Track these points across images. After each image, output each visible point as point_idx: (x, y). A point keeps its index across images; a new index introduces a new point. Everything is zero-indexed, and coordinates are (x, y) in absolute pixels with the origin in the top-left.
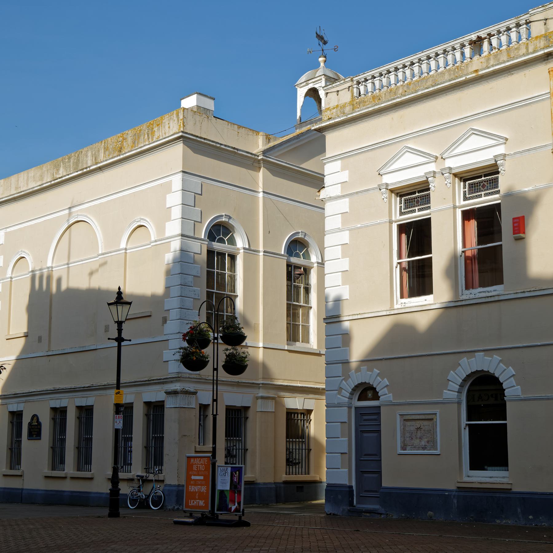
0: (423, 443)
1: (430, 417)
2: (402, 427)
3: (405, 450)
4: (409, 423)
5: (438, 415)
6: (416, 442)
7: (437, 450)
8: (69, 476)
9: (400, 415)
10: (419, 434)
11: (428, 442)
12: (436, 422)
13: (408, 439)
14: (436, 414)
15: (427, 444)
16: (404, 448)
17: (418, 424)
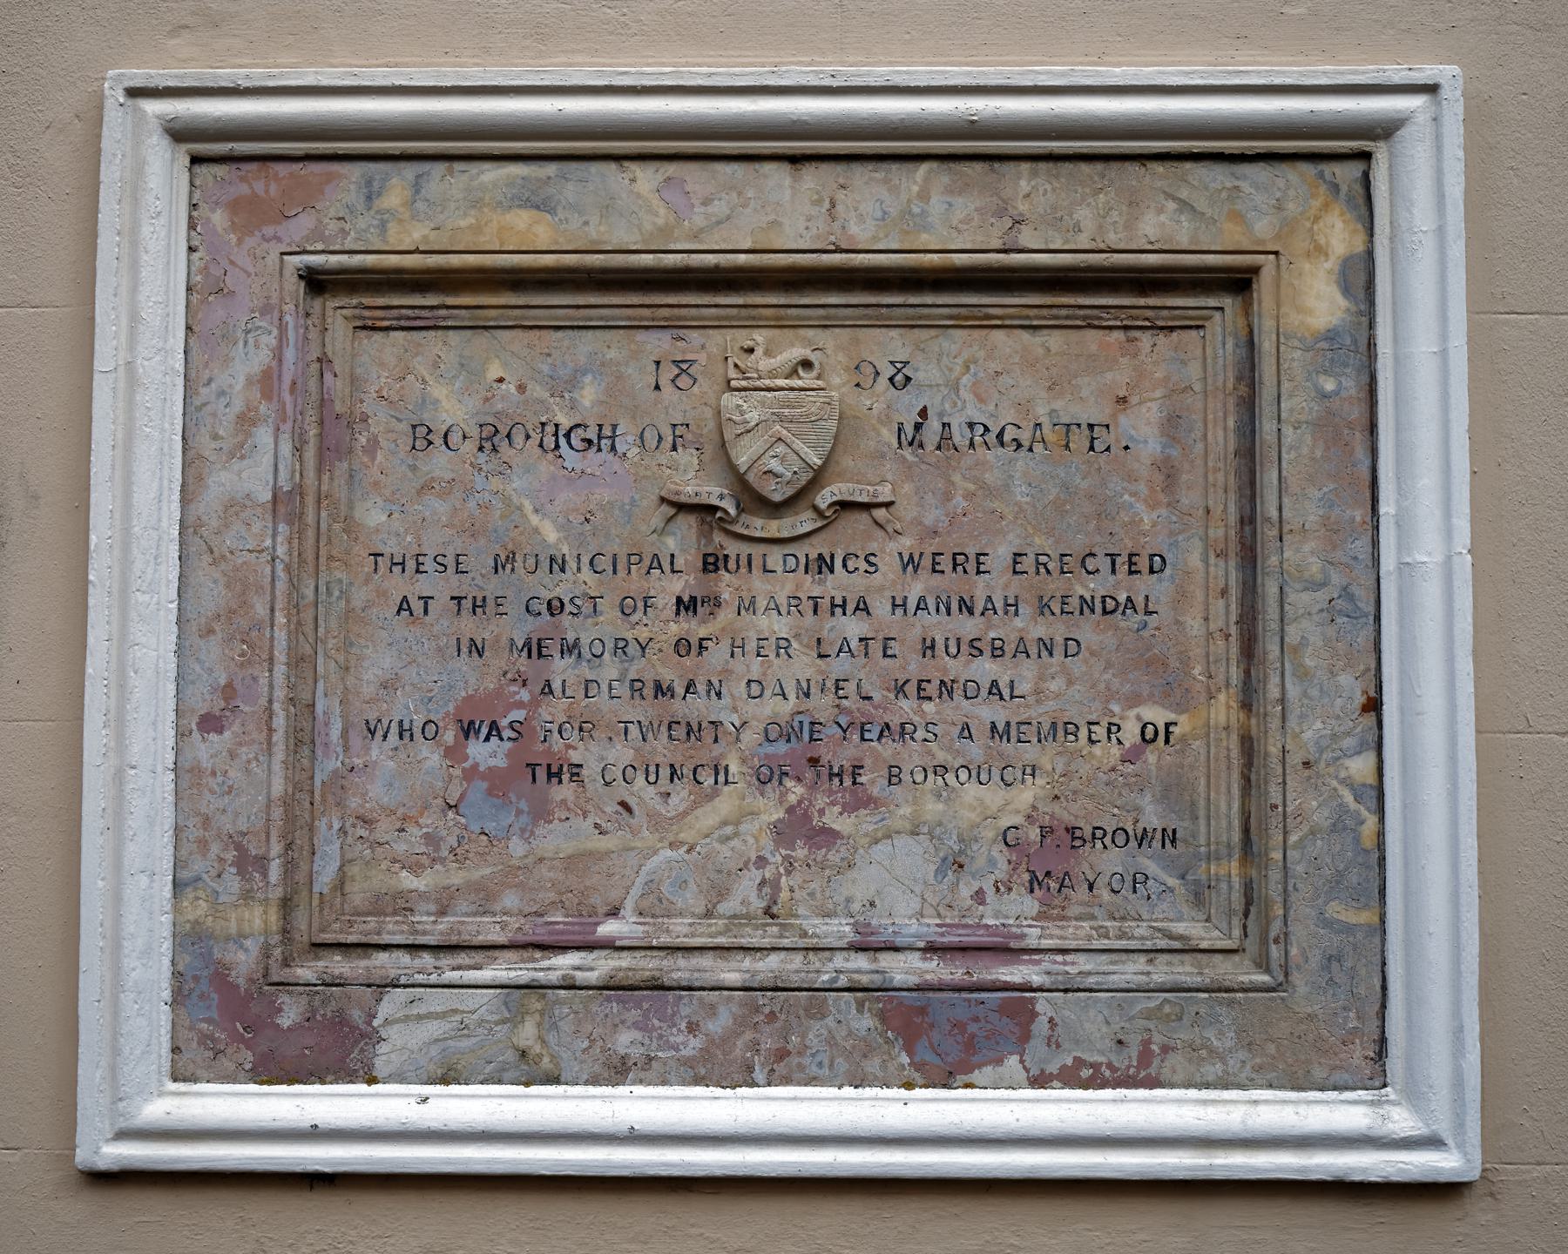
0: (892, 885)
1: (1157, 221)
2: (257, 472)
3: (340, 1053)
4: (447, 376)
5: (1426, 187)
6: (675, 857)
7: (1372, 1066)
8: (1236, 716)
9: (204, 148)
10: (772, 643)
11: (1050, 859)
12: (1357, 347)
13: (390, 776)
14: (1344, 155)
15: (1015, 911)
16: (276, 1002)
17: (783, 393)
